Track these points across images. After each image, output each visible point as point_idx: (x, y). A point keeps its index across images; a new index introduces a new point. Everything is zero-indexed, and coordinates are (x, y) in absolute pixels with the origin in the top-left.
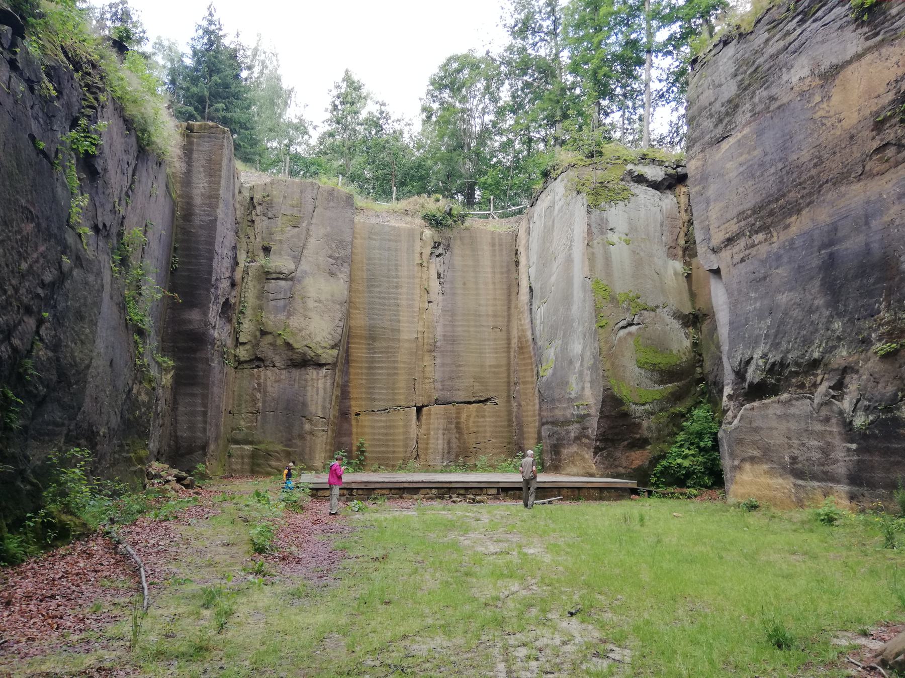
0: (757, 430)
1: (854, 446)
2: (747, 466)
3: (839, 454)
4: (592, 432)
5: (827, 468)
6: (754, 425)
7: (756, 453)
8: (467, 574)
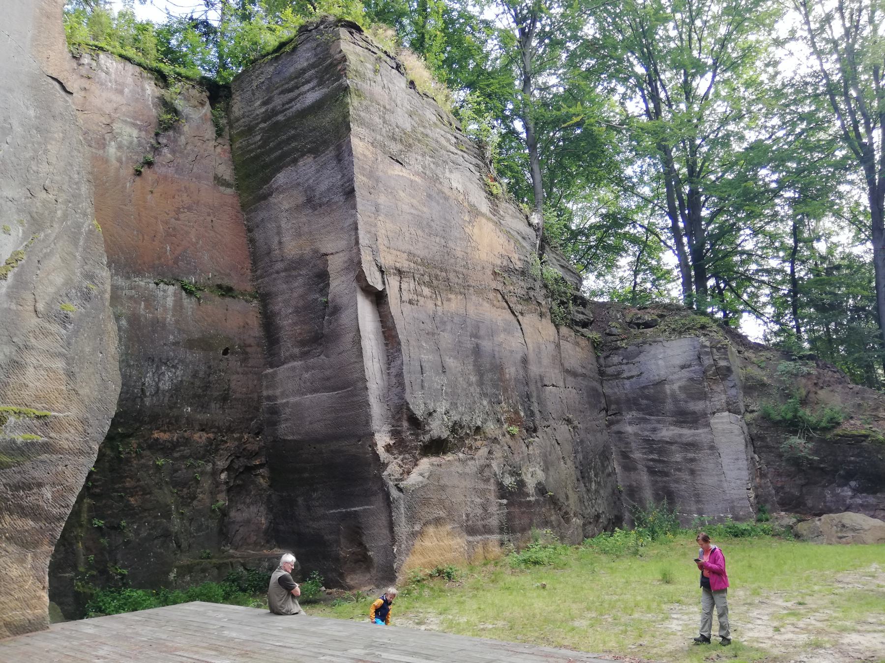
0: (443, 488)
1: (505, 501)
2: (431, 530)
3: (493, 509)
4: (58, 498)
5: (486, 522)
6: (442, 482)
7: (442, 514)
8: (737, 459)
